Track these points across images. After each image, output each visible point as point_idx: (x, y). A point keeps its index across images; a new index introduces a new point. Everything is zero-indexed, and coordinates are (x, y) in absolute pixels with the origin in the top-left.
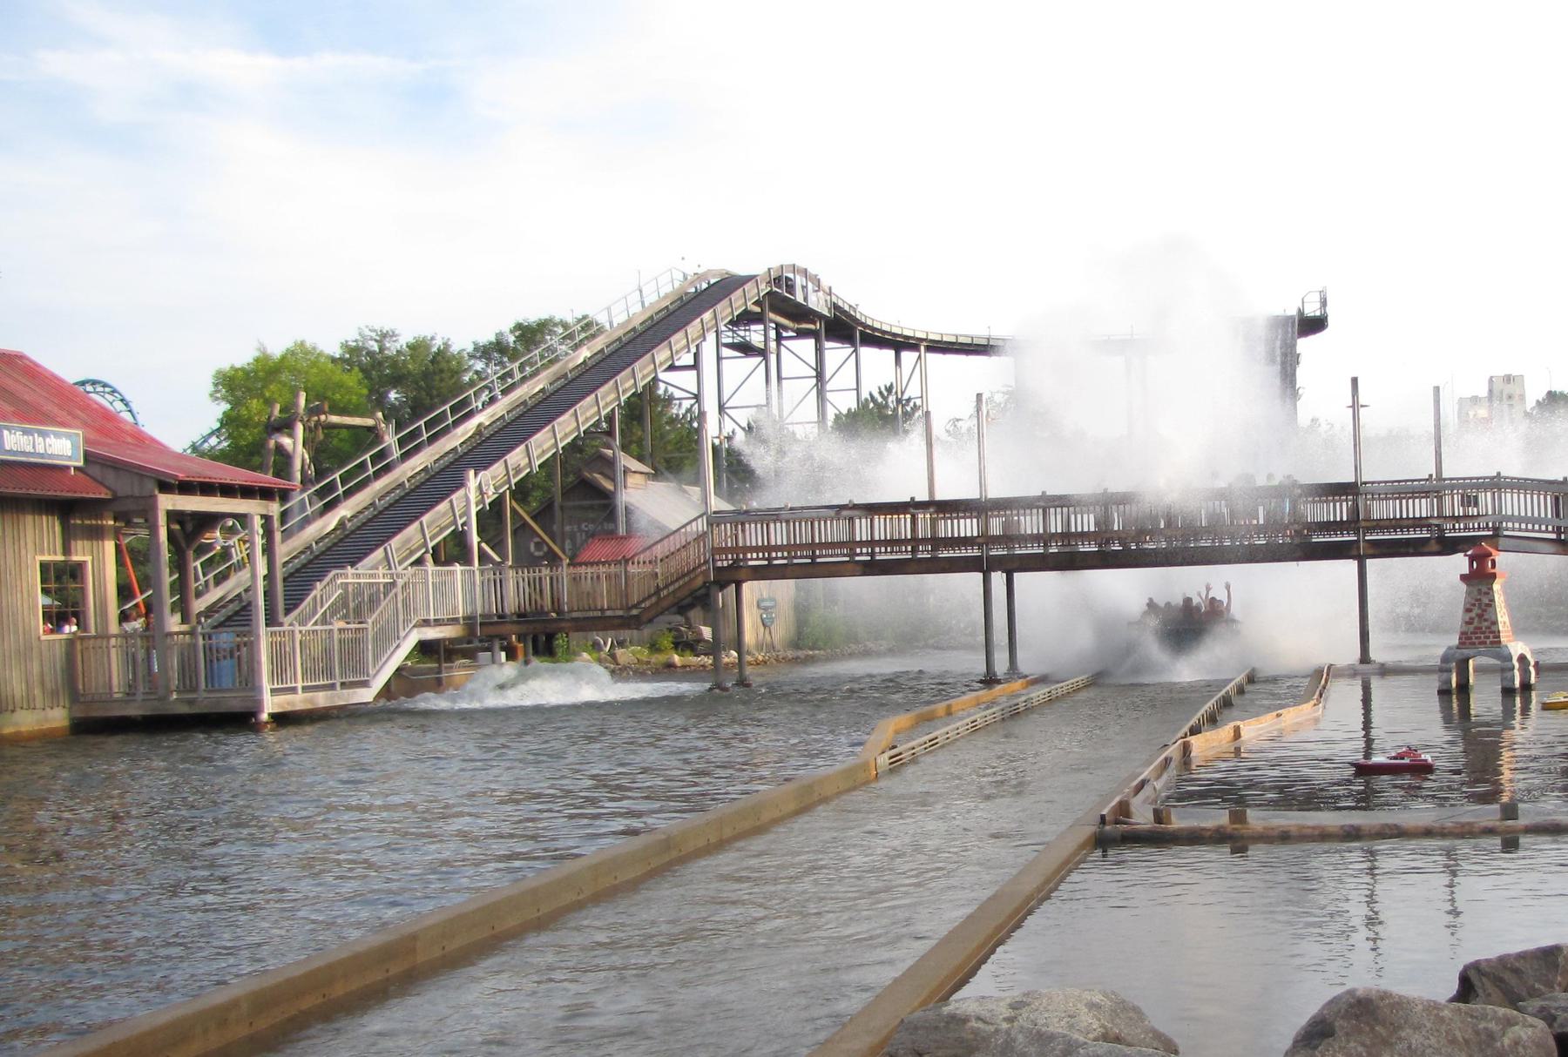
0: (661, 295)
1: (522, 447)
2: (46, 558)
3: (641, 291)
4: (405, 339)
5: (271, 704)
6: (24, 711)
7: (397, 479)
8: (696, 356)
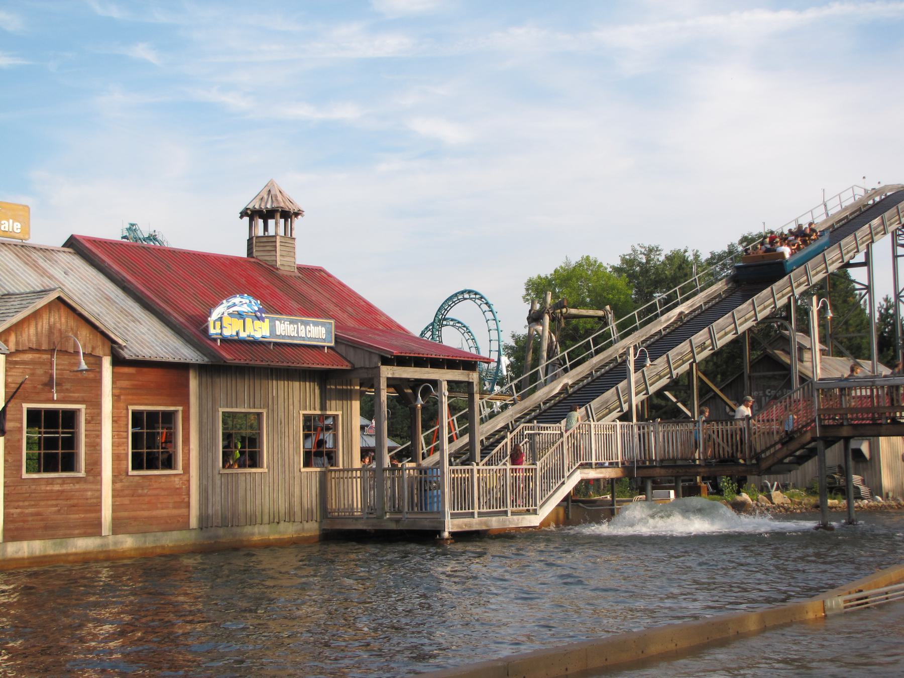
0: (843, 207)
1: (706, 329)
2: (308, 412)
3: (825, 206)
4: (666, 250)
5: (451, 525)
6: (286, 523)
7: (611, 355)
8: (868, 255)
